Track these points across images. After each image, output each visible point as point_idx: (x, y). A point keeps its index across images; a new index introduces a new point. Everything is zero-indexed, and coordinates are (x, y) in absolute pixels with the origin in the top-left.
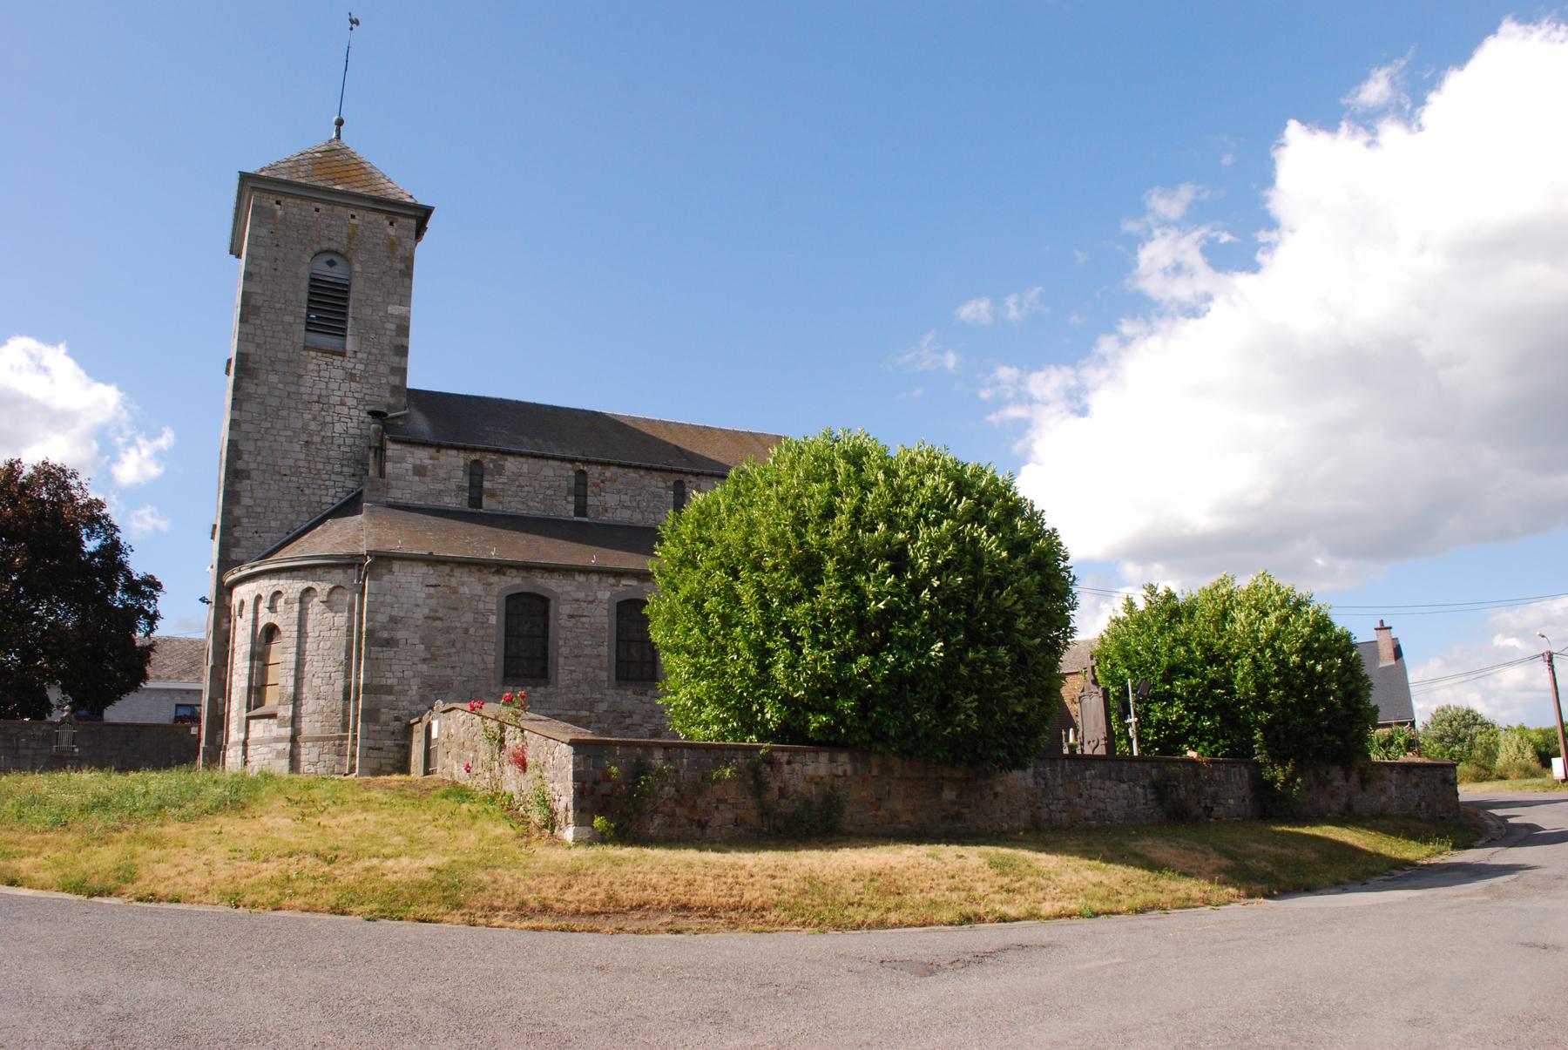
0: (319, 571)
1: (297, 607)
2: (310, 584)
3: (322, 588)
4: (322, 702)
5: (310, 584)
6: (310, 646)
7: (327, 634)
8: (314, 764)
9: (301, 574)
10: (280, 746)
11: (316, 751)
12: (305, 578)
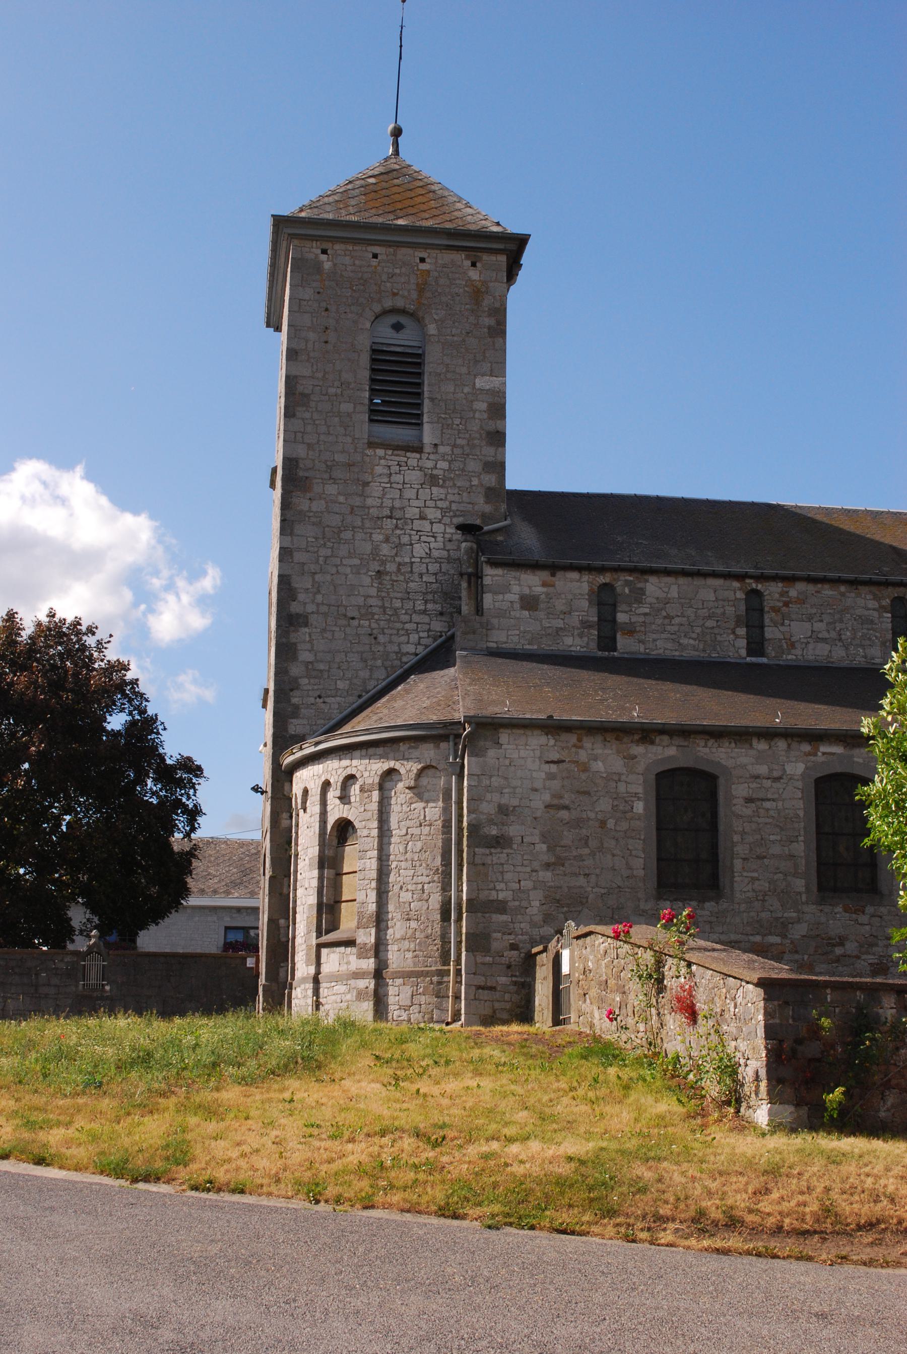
0: (403, 747)
1: (376, 795)
2: (392, 764)
3: (408, 768)
4: (414, 924)
5: (392, 764)
6: (395, 848)
7: (416, 831)
8: (406, 1009)
9: (380, 750)
10: (362, 984)
11: (407, 991)
12: (384, 757)
